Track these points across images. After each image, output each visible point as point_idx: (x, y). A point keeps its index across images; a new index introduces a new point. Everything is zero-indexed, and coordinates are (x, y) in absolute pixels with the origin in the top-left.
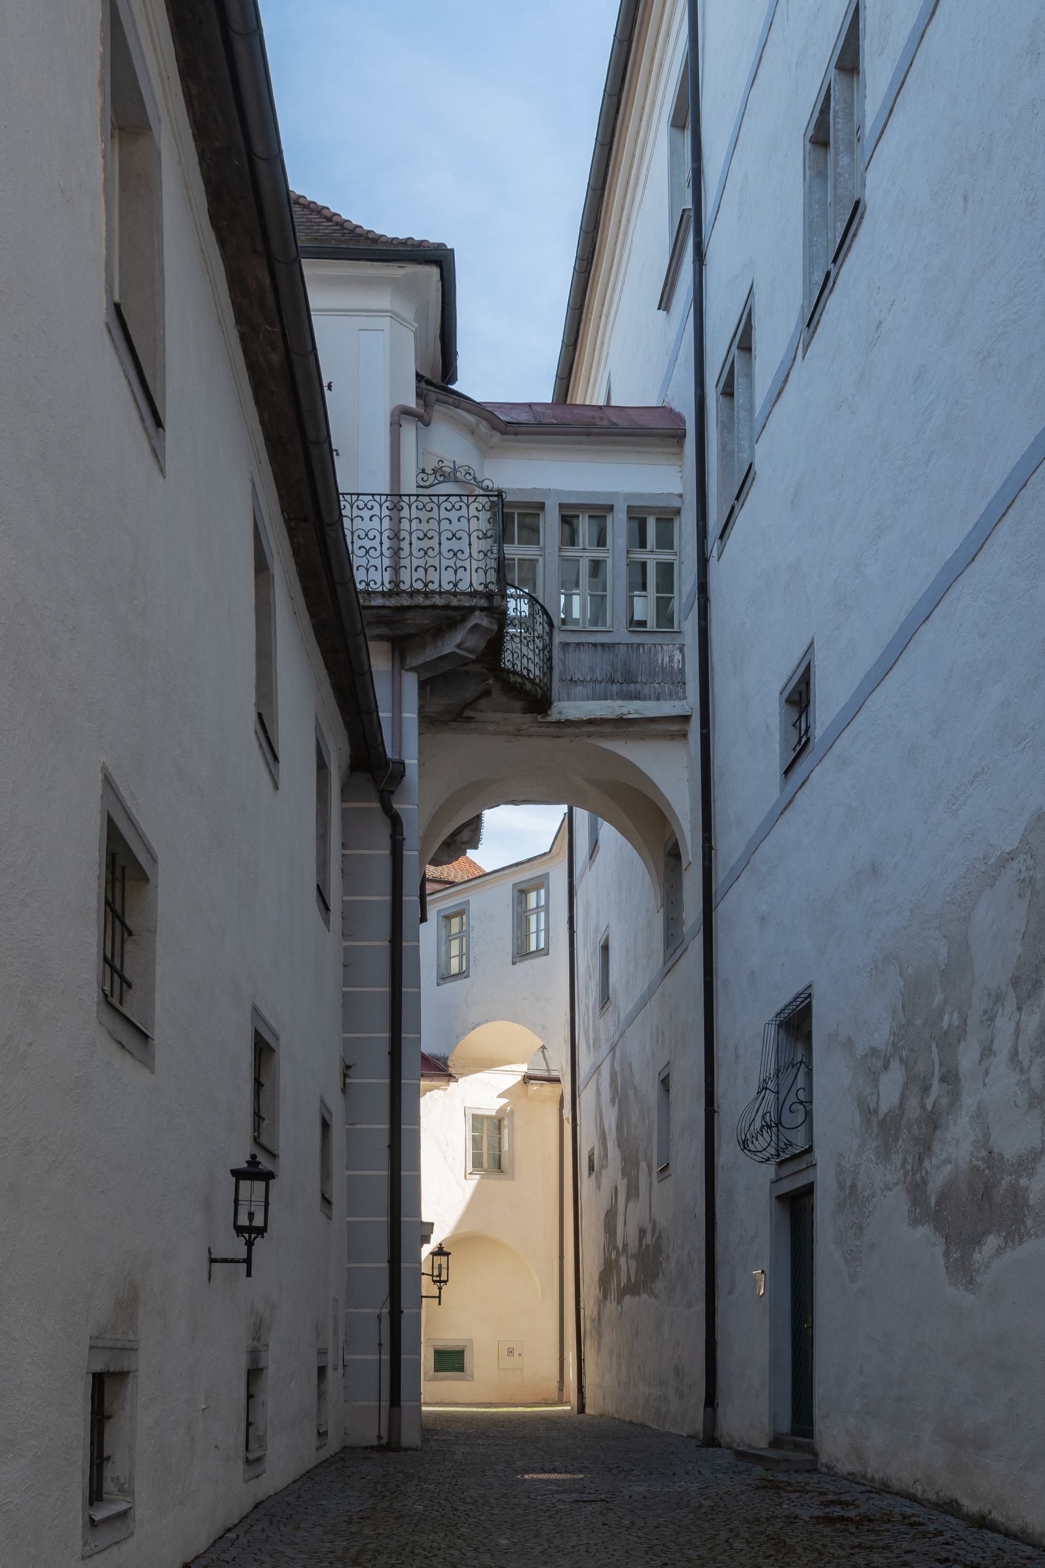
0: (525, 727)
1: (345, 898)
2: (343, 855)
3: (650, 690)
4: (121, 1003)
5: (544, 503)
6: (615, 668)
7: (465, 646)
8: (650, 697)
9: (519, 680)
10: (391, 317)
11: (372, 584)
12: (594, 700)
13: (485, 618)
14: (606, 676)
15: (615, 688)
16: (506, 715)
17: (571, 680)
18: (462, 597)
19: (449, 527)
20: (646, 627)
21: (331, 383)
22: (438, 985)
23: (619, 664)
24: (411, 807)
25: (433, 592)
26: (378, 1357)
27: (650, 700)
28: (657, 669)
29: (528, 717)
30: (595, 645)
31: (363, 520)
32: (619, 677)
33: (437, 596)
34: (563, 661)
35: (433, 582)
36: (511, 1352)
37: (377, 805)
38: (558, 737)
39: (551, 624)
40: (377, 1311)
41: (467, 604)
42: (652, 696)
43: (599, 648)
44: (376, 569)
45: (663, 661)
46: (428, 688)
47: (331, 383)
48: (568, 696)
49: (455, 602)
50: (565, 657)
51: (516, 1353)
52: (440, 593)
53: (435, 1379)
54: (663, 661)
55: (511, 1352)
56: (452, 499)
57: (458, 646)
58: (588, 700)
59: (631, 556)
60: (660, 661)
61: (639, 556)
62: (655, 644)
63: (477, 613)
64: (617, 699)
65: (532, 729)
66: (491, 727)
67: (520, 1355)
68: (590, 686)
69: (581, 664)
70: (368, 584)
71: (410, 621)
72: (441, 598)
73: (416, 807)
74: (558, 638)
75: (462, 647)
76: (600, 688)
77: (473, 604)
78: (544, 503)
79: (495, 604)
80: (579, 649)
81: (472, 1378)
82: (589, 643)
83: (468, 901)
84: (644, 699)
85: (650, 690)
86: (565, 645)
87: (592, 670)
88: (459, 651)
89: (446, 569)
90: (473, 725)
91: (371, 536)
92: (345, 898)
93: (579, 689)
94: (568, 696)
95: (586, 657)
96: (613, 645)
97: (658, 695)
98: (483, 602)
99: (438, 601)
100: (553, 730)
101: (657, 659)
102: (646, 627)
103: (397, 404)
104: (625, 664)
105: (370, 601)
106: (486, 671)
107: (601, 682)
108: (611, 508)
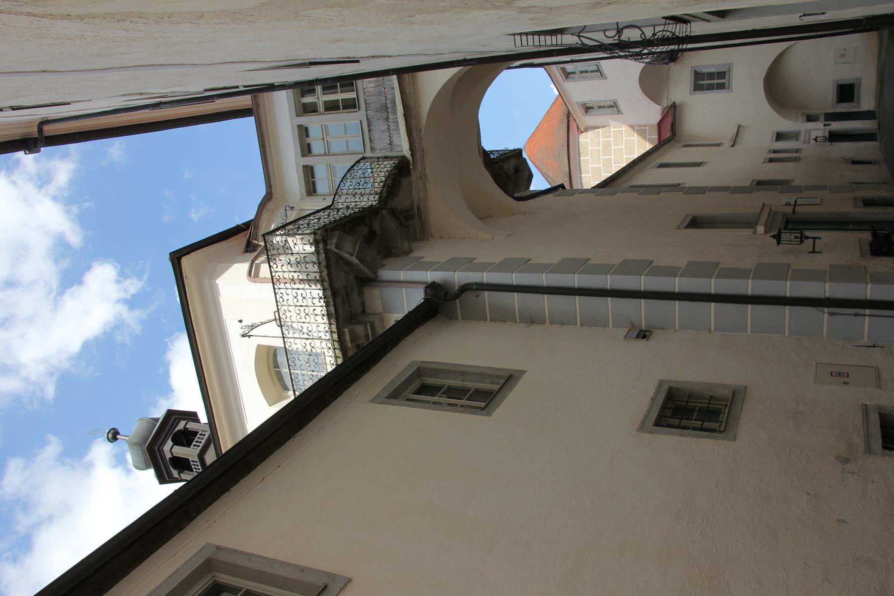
0: (418, 174)
1: (518, 321)
2: (491, 321)
3: (389, 94)
4: (664, 192)
5: (303, 166)
6: (380, 117)
7: (351, 250)
8: (392, 94)
9: (385, 189)
10: (211, 279)
11: (323, 312)
12: (399, 130)
13: (332, 241)
14: (385, 122)
15: (391, 116)
16: (413, 186)
17: (390, 144)
18: (321, 258)
19: (285, 265)
20: (355, 98)
21: (239, 321)
22: (622, 114)
23: (377, 115)
24: (456, 276)
25: (321, 276)
26: (867, 318)
27: (394, 94)
28: (377, 91)
29: (412, 172)
30: (369, 131)
31: (291, 316)
32: (385, 114)
33: (323, 274)
34: (381, 150)
35: (315, 277)
36: (843, 56)
37: (457, 300)
38: (423, 151)
39: (363, 158)
40: (826, 316)
41: (324, 256)
42: (392, 92)
43: (371, 127)
44: (315, 310)
45: (372, 87)
46: (394, 251)
47: (239, 321)
48: (399, 146)
49: (324, 263)
50: (379, 149)
51: (844, 52)
52: (320, 272)
53: (859, 102)
54: (372, 87)
55: (843, 56)
56: (271, 265)
57: (352, 255)
58: (400, 133)
59: (322, 112)
60: (373, 89)
61: (321, 107)
62: (364, 93)
63: (328, 247)
64: (397, 115)
65: (420, 170)
66: (422, 195)
67: (845, 50)
68: (392, 132)
69: (380, 141)
70: (323, 315)
71: (344, 283)
72: (323, 272)
73: (456, 273)
74: (369, 154)
75: (352, 252)
76: (392, 126)
77: (323, 252)
78: (303, 166)
79: (321, 238)
80: (373, 140)
81: (859, 80)
82: (369, 134)
83: (576, 103)
84: (395, 97)
85: (389, 94)
86: (372, 149)
87: (383, 131)
88: (355, 254)
89: (307, 268)
90: (422, 206)
91: (299, 312)
92: (518, 321)
93: (394, 139)
94: (399, 146)
95: (376, 136)
96: (368, 119)
97: (391, 88)
98: (321, 246)
99: (325, 273)
100: (418, 156)
101: (372, 91)
102: (355, 98)
103: (246, 279)
104: (377, 111)
105: (332, 314)
106: (379, 215)
107: (389, 125)
108: (300, 127)
